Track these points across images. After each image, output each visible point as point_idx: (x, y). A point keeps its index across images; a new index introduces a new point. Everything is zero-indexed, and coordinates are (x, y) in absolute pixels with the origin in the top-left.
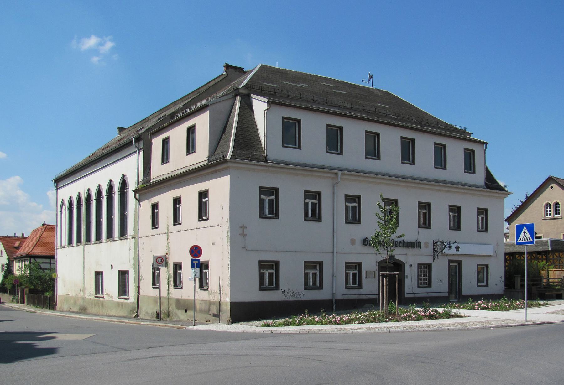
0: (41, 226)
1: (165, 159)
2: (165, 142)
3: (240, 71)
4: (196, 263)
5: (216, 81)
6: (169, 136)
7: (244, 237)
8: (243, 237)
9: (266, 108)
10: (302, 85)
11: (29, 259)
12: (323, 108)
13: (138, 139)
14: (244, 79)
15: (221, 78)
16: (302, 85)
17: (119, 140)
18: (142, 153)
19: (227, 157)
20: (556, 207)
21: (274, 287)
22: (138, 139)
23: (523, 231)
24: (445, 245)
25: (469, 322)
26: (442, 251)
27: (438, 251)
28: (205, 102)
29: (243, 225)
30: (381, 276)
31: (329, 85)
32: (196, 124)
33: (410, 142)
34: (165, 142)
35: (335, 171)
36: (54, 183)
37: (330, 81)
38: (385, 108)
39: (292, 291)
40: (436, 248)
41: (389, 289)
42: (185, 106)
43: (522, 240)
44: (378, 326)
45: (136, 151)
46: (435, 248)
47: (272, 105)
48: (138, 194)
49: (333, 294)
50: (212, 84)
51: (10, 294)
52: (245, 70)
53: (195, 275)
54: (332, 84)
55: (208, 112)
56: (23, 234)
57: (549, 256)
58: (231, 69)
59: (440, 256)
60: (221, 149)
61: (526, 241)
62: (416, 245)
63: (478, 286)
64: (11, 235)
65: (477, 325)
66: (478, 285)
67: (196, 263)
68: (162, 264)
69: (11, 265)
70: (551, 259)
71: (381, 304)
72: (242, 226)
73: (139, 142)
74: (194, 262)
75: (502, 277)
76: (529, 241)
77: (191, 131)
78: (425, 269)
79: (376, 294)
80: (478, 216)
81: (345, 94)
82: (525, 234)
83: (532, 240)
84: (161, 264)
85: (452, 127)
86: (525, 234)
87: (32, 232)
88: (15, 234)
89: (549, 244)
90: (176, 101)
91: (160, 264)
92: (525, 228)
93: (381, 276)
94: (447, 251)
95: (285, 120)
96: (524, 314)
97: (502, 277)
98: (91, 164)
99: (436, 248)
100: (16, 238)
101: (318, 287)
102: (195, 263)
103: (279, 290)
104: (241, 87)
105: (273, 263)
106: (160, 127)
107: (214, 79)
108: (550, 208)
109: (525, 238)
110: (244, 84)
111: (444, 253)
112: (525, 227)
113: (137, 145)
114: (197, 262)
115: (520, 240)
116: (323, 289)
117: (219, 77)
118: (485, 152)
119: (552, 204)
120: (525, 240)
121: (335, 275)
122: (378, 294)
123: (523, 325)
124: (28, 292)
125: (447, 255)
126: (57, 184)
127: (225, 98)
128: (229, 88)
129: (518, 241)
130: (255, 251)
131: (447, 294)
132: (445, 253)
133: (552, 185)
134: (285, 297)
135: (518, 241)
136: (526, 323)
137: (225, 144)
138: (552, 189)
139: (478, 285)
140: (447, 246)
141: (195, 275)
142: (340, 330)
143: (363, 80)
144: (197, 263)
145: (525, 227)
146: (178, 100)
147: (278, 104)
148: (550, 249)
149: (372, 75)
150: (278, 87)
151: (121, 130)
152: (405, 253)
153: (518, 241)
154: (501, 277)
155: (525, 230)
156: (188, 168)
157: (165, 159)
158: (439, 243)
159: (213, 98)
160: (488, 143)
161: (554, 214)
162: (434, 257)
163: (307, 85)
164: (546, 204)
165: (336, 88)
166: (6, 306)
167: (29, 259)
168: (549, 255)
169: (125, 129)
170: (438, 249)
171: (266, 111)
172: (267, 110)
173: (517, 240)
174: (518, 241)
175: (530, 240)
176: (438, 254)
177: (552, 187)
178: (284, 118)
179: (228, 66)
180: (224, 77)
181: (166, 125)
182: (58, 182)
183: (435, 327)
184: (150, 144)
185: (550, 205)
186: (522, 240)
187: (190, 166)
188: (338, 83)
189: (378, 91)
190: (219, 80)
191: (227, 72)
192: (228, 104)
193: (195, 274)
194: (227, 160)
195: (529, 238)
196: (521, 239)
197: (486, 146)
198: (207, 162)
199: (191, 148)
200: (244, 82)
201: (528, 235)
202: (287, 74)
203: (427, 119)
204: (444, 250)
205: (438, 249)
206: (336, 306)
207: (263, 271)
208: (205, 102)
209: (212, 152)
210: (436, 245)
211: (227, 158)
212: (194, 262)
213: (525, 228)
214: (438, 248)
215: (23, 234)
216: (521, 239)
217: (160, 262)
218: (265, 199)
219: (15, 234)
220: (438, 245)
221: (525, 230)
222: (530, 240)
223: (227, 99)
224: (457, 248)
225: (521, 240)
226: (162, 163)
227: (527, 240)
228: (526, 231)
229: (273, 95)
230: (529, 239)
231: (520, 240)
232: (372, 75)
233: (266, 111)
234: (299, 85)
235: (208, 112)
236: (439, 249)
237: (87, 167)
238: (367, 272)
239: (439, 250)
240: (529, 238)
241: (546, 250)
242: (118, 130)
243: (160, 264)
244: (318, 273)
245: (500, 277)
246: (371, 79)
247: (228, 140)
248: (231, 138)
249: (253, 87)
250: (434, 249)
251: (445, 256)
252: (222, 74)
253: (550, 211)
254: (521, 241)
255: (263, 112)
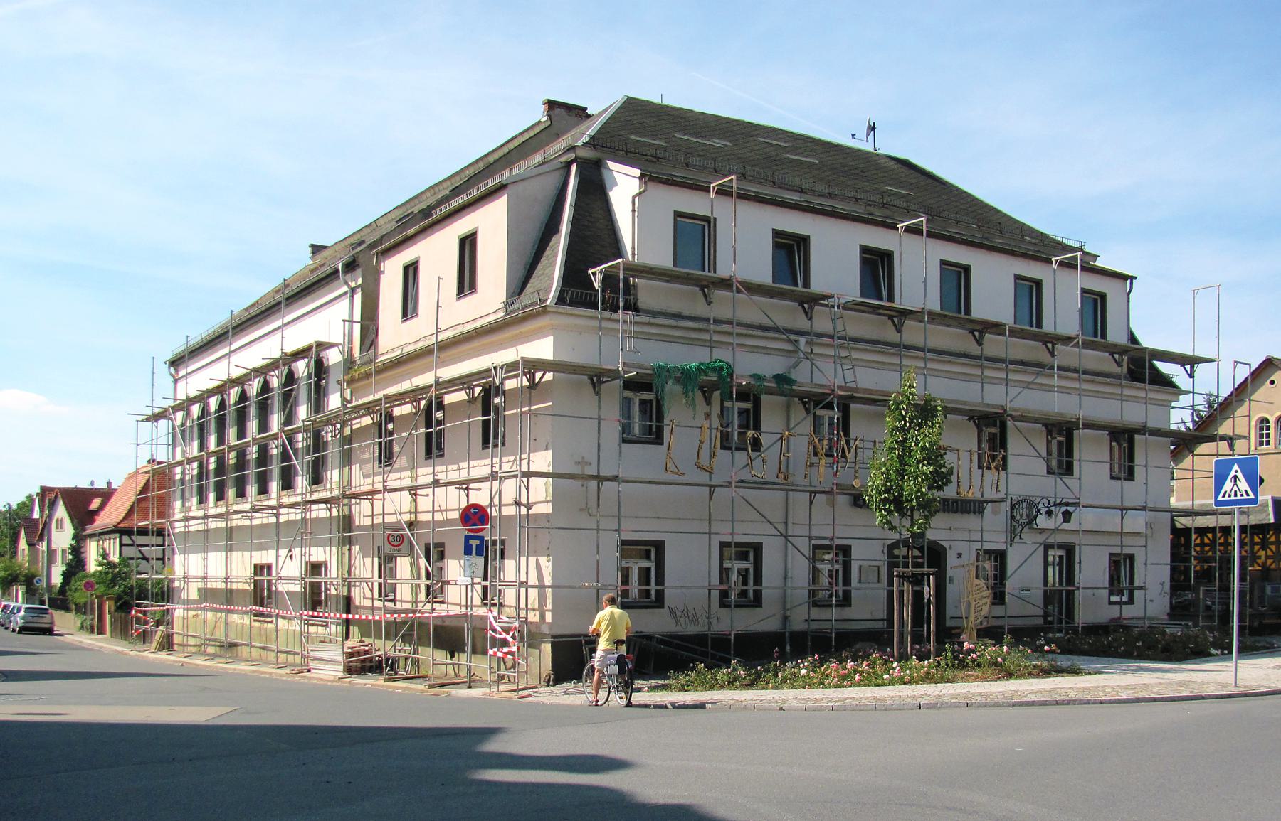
0: (146, 464)
1: (409, 309)
2: (411, 271)
3: (580, 113)
4: (474, 543)
5: (526, 136)
6: (419, 257)
7: (585, 486)
8: (583, 485)
9: (637, 191)
10: (718, 143)
11: (118, 535)
12: (767, 191)
13: (351, 266)
14: (588, 128)
15: (537, 130)
16: (718, 143)
17: (312, 271)
18: (358, 297)
19: (547, 300)
20: (1261, 429)
21: (652, 602)
22: (351, 266)
23: (1233, 473)
24: (1037, 507)
25: (1102, 687)
26: (1030, 522)
27: (1023, 521)
28: (503, 177)
29: (583, 458)
30: (897, 576)
31: (779, 143)
32: (477, 228)
33: (960, 272)
34: (411, 271)
35: (793, 337)
36: (169, 368)
37: (782, 136)
38: (903, 196)
39: (691, 612)
40: (1018, 515)
41: (246, 675)
42: (456, 192)
43: (1230, 496)
44: (891, 694)
45: (346, 293)
46: (1015, 514)
47: (650, 185)
48: (349, 390)
49: (785, 619)
50: (516, 143)
51: (76, 613)
52: (589, 112)
53: (474, 572)
54: (785, 142)
55: (506, 197)
56: (109, 484)
57: (1268, 536)
58: (559, 110)
59: (1026, 533)
60: (535, 284)
61: (1239, 497)
62: (972, 507)
63: (1111, 603)
64: (84, 484)
65: (1122, 695)
66: (1111, 600)
67: (474, 543)
68: (400, 547)
69: (82, 550)
70: (1272, 543)
71: (897, 643)
72: (580, 460)
73: (352, 272)
74: (471, 542)
75: (1164, 582)
76: (1245, 497)
77: (468, 245)
78: (993, 563)
79: (883, 620)
80: (1111, 444)
81: (814, 164)
82: (1235, 481)
83: (1252, 496)
84: (397, 548)
85: (1054, 241)
86: (1235, 481)
87: (127, 479)
88: (92, 483)
89: (1271, 509)
90: (436, 185)
91: (396, 546)
92: (1236, 467)
93: (897, 576)
94: (1042, 521)
95: (679, 219)
96: (1233, 673)
97: (1164, 582)
98: (248, 324)
99: (1018, 515)
100: (94, 493)
101: (750, 601)
102: (471, 545)
103: (663, 608)
104: (580, 143)
105: (650, 546)
106: (399, 237)
107: (522, 133)
108: (1268, 429)
109: (1236, 492)
110: (588, 139)
111: (1035, 526)
112: (1236, 465)
113: (348, 277)
114: (478, 542)
115: (1224, 496)
116: (761, 606)
117: (532, 127)
118: (1129, 298)
119: (1272, 420)
120: (1236, 495)
121: (789, 575)
122: (885, 617)
123: (1230, 696)
124: (113, 608)
125: (1042, 531)
126: (177, 372)
127: (545, 168)
128: (554, 149)
129: (1220, 498)
130: (610, 516)
131: (1040, 621)
132: (1039, 527)
133: (1272, 378)
134: (677, 623)
135: (1220, 498)
136: (1236, 691)
137: (543, 274)
138: (1274, 385)
139: (1111, 600)
140: (1044, 510)
141: (474, 572)
142: (803, 702)
143: (853, 135)
144: (477, 546)
145: (1236, 465)
146: (441, 182)
147: (664, 183)
148: (1272, 521)
149: (874, 123)
150: (664, 147)
151: (316, 249)
152: (948, 527)
153: (1218, 499)
154: (1162, 584)
155: (1236, 471)
156: (460, 329)
157: (409, 309)
158: (1025, 504)
159: (520, 169)
160: (1135, 278)
161: (1258, 444)
162: (1013, 536)
163: (728, 144)
164: (1260, 418)
165: (793, 150)
166: (68, 641)
167: (118, 535)
168: (1268, 533)
169: (325, 247)
170: (1021, 517)
171: (637, 199)
172: (640, 194)
173: (1217, 495)
174: (1218, 499)
175: (1248, 495)
176: (1023, 528)
177: (1272, 382)
178: (678, 214)
179: (552, 105)
180: (542, 126)
181: (411, 232)
182: (178, 365)
183: (1025, 697)
184: (377, 273)
185: (1268, 421)
186: (1230, 496)
187: (465, 325)
188: (798, 139)
189: (887, 160)
190: (532, 133)
191: (549, 116)
192: (552, 182)
193: (473, 569)
194: (549, 309)
195: (1246, 491)
196: (1225, 492)
197: (1131, 283)
198: (501, 314)
199: (467, 282)
200: (588, 133)
201: (1243, 485)
202: (685, 118)
203: (999, 221)
204: (1035, 519)
205: (1021, 517)
206: (790, 646)
207: (627, 565)
208: (503, 177)
209: (514, 292)
210: (1017, 509)
211: (548, 303)
212: (471, 542)
213: (1236, 467)
214: (1021, 515)
215: (109, 484)
216: (1225, 492)
217: (396, 543)
218: (633, 399)
219: (92, 483)
220: (1023, 509)
221: (1236, 471)
222: (1248, 495)
223: (548, 172)
224: (1067, 516)
225: (1227, 495)
226: (403, 318)
227: (1242, 495)
228: (1240, 475)
229: (653, 162)
230: (1244, 494)
231: (1224, 496)
232: (874, 123)
233: (637, 199)
234: (711, 143)
235: (506, 197)
236: (1024, 517)
237: (241, 330)
238: (862, 568)
239: (1024, 520)
240: (1246, 491)
241: (1264, 522)
242: (309, 250)
243: (396, 546)
244: (751, 571)
245: (1161, 584)
246: (872, 132)
247: (551, 264)
248: (558, 246)
249: (608, 145)
250: (1012, 517)
251: (1038, 535)
252: (540, 122)
253: (1268, 436)
254: (1226, 498)
255: (630, 200)
